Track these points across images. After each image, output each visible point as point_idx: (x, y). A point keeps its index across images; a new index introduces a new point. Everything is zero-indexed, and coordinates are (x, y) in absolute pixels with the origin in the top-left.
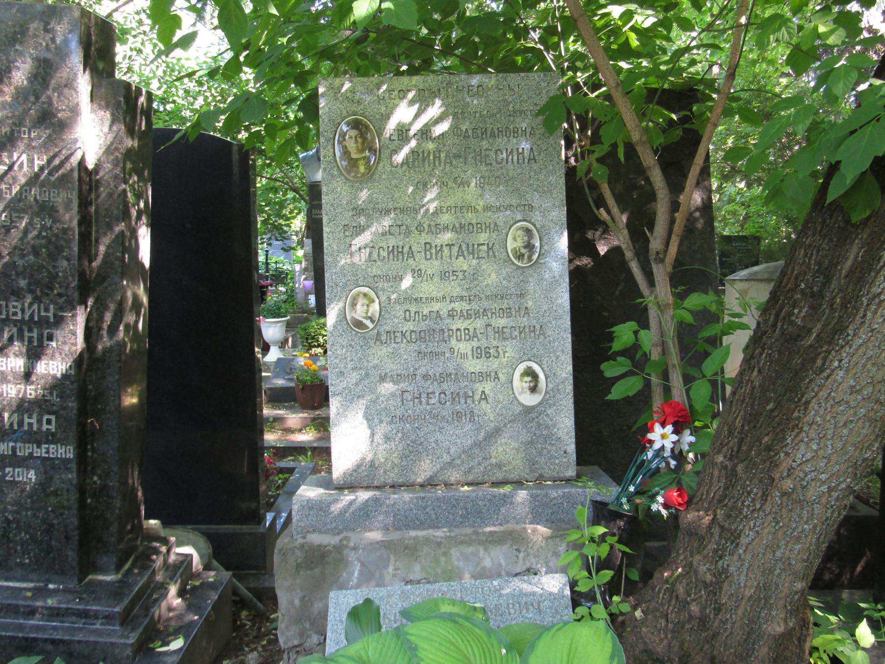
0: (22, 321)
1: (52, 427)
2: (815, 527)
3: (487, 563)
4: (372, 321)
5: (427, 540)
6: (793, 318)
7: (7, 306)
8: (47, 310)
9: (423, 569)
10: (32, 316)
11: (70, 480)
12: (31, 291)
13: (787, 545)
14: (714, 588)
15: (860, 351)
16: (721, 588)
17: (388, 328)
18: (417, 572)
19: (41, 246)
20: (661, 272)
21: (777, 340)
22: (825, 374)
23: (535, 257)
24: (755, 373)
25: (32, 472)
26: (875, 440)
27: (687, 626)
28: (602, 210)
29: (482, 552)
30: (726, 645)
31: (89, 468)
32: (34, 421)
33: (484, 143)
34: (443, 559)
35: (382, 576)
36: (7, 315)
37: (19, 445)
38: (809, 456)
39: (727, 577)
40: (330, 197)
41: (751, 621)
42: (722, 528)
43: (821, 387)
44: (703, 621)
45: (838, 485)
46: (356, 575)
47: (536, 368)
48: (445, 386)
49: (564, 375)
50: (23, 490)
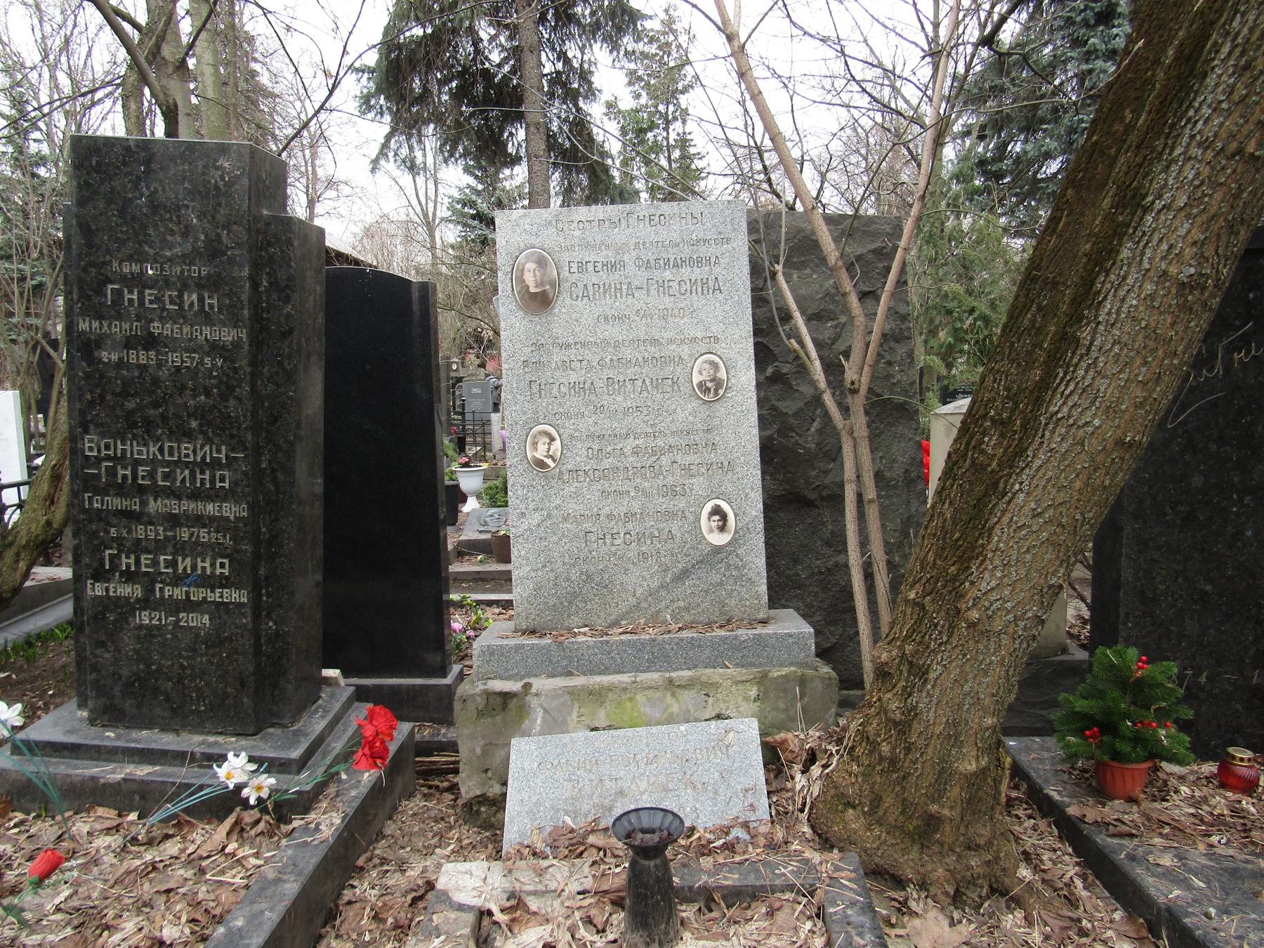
0: (194, 463)
1: (226, 571)
2: (1003, 658)
3: (675, 708)
4: (554, 460)
5: (611, 688)
6: (984, 446)
7: (179, 448)
8: (219, 451)
9: (608, 716)
10: (204, 458)
11: (245, 625)
12: (202, 432)
13: (974, 679)
14: (902, 727)
15: (1040, 474)
16: (910, 726)
17: (570, 467)
18: (601, 718)
19: (213, 386)
20: (858, 403)
21: (967, 470)
22: (1007, 498)
23: (721, 392)
24: (947, 505)
25: (207, 617)
26: (1061, 565)
27: (878, 768)
28: (793, 341)
29: (669, 699)
30: (917, 785)
31: (264, 613)
32: (207, 565)
33: (668, 273)
34: (628, 705)
35: (565, 722)
36: (179, 457)
37: (192, 589)
38: (993, 584)
39: (916, 715)
40: (508, 333)
41: (942, 760)
42: (911, 663)
43: (1004, 512)
44: (893, 761)
45: (1025, 613)
46: (539, 722)
47: (725, 506)
48: (630, 526)
49: (754, 513)
50: (198, 635)
